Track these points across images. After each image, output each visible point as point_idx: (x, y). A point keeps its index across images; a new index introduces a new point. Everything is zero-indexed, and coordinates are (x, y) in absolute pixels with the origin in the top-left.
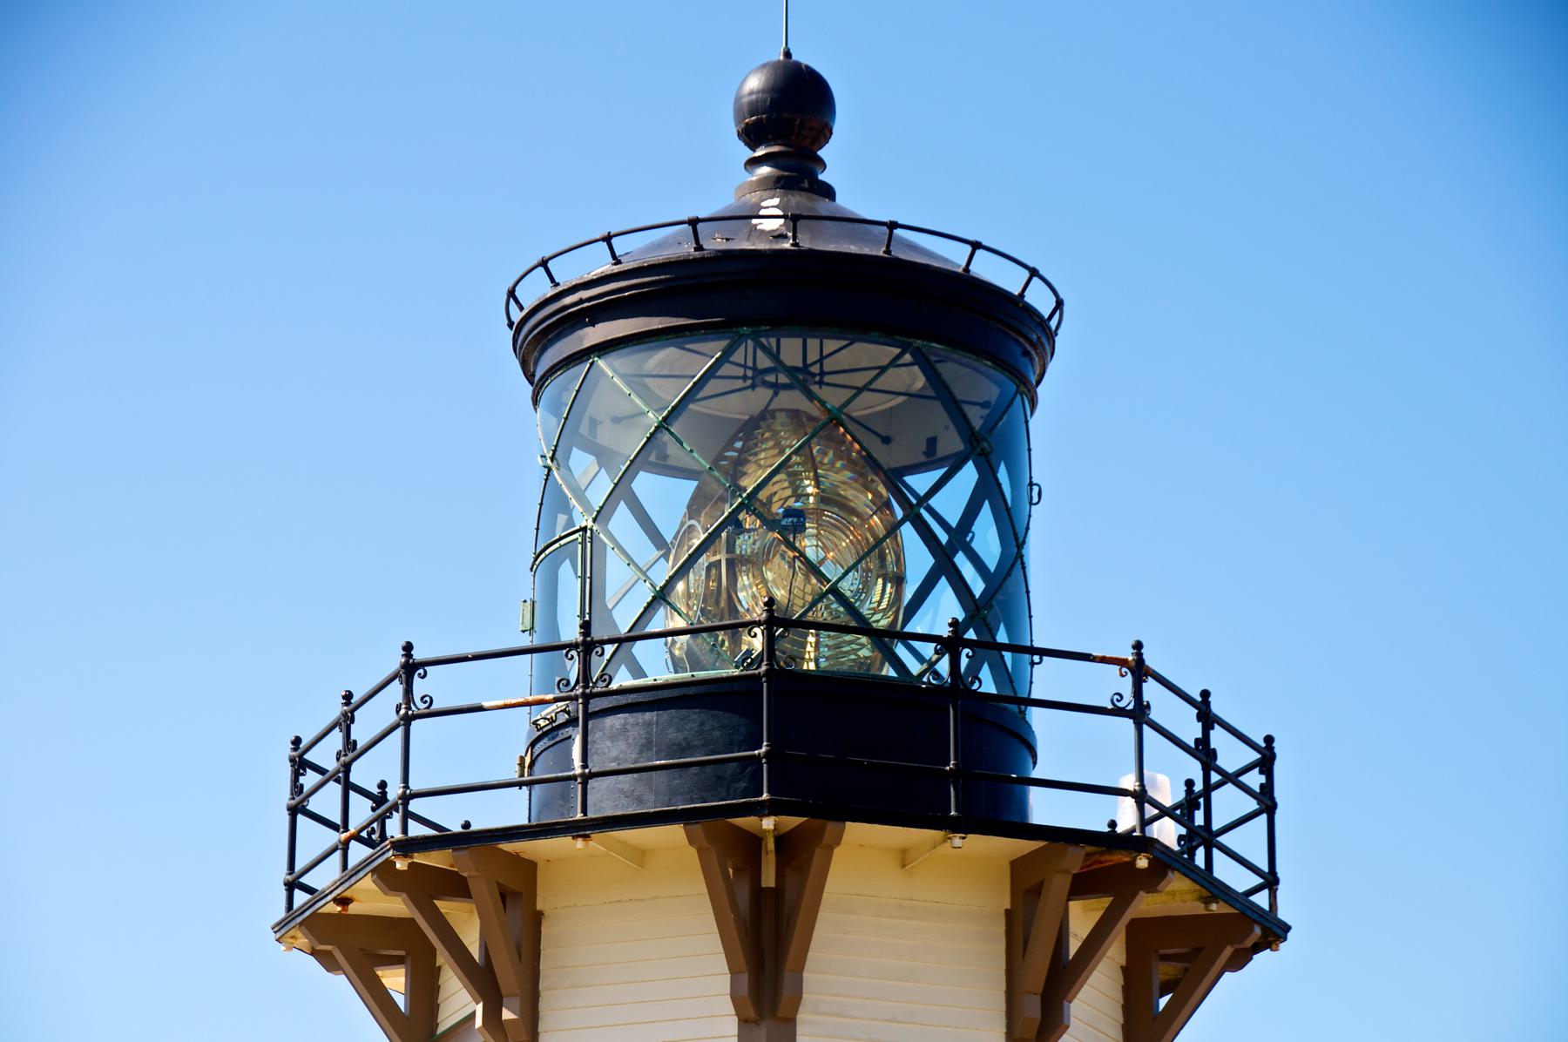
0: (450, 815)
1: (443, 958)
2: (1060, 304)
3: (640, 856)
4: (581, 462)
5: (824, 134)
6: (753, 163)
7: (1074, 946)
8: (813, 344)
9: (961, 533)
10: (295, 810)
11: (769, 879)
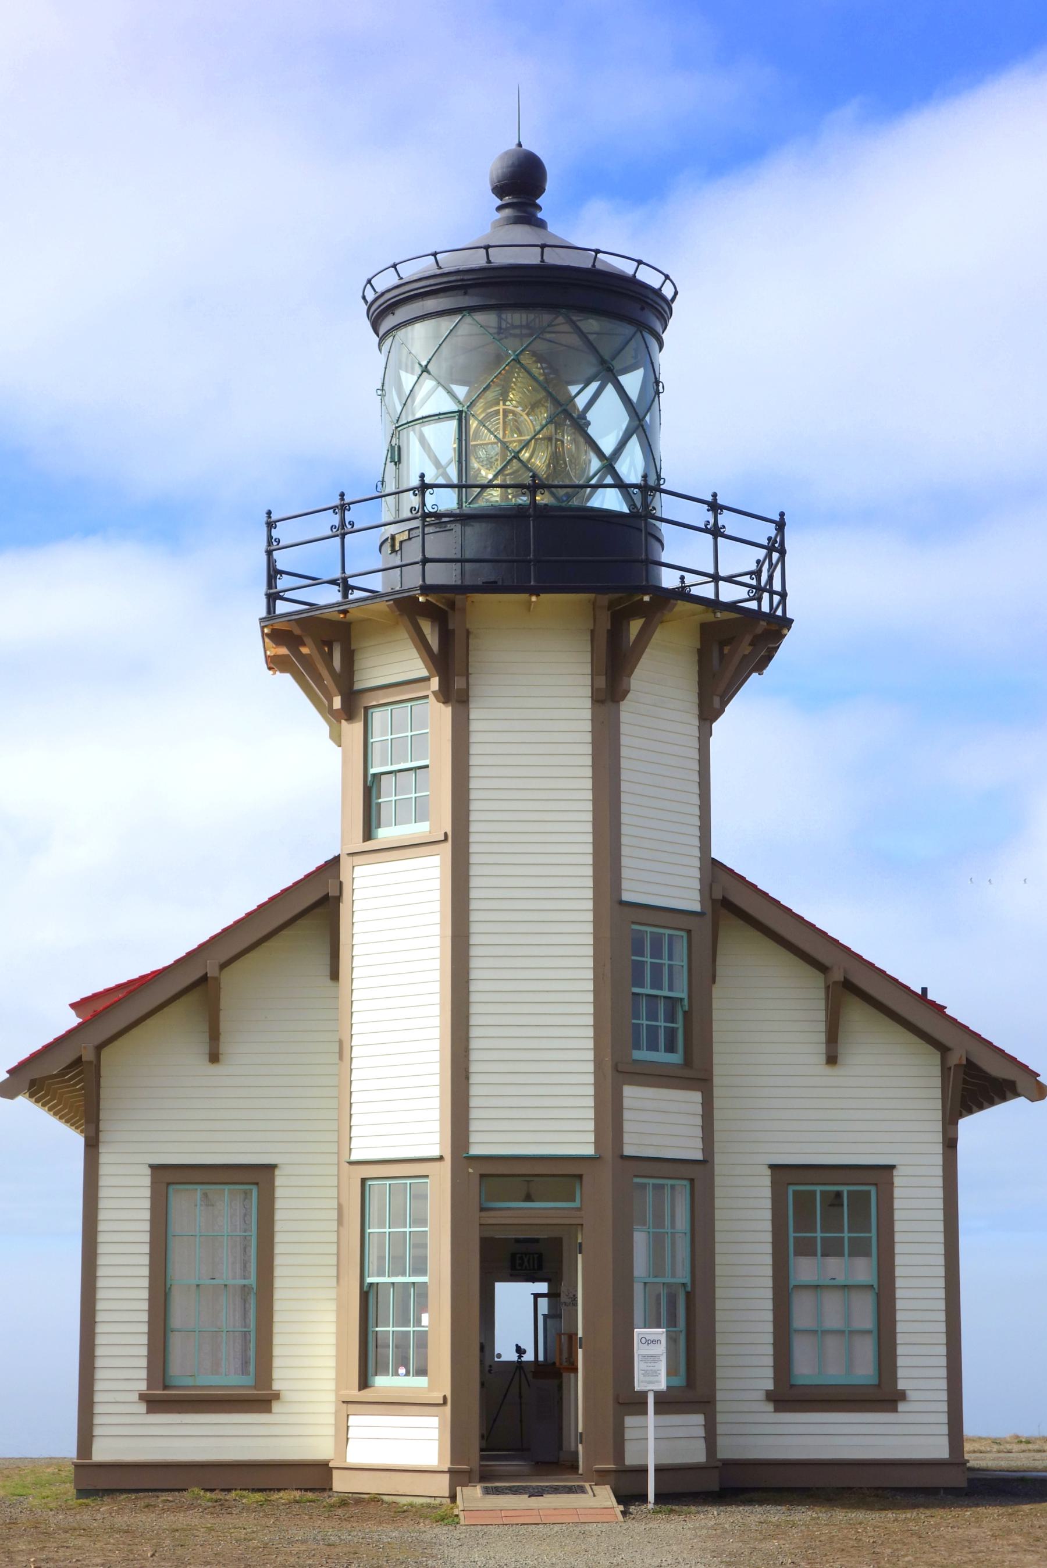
2: (676, 293)
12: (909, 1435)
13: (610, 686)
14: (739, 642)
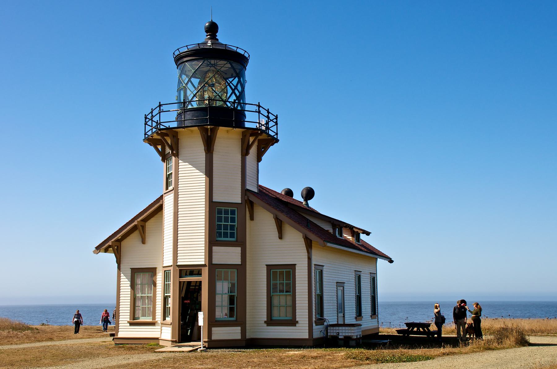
0: (167, 125)
1: (166, 144)
3: (192, 131)
4: (184, 77)
5: (217, 32)
6: (207, 35)
7: (250, 143)
8: (216, 61)
9: (236, 87)
10: (145, 124)
11: (209, 134)
12: (301, 331)
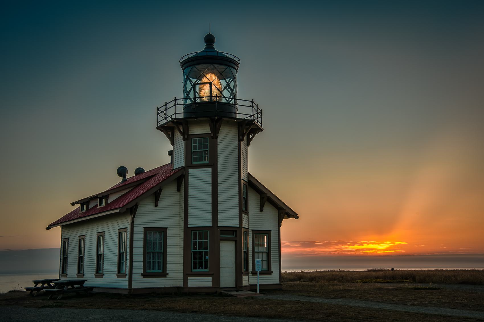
5: (213, 42)
12: (273, 279)
13: (240, 140)
14: (248, 129)
